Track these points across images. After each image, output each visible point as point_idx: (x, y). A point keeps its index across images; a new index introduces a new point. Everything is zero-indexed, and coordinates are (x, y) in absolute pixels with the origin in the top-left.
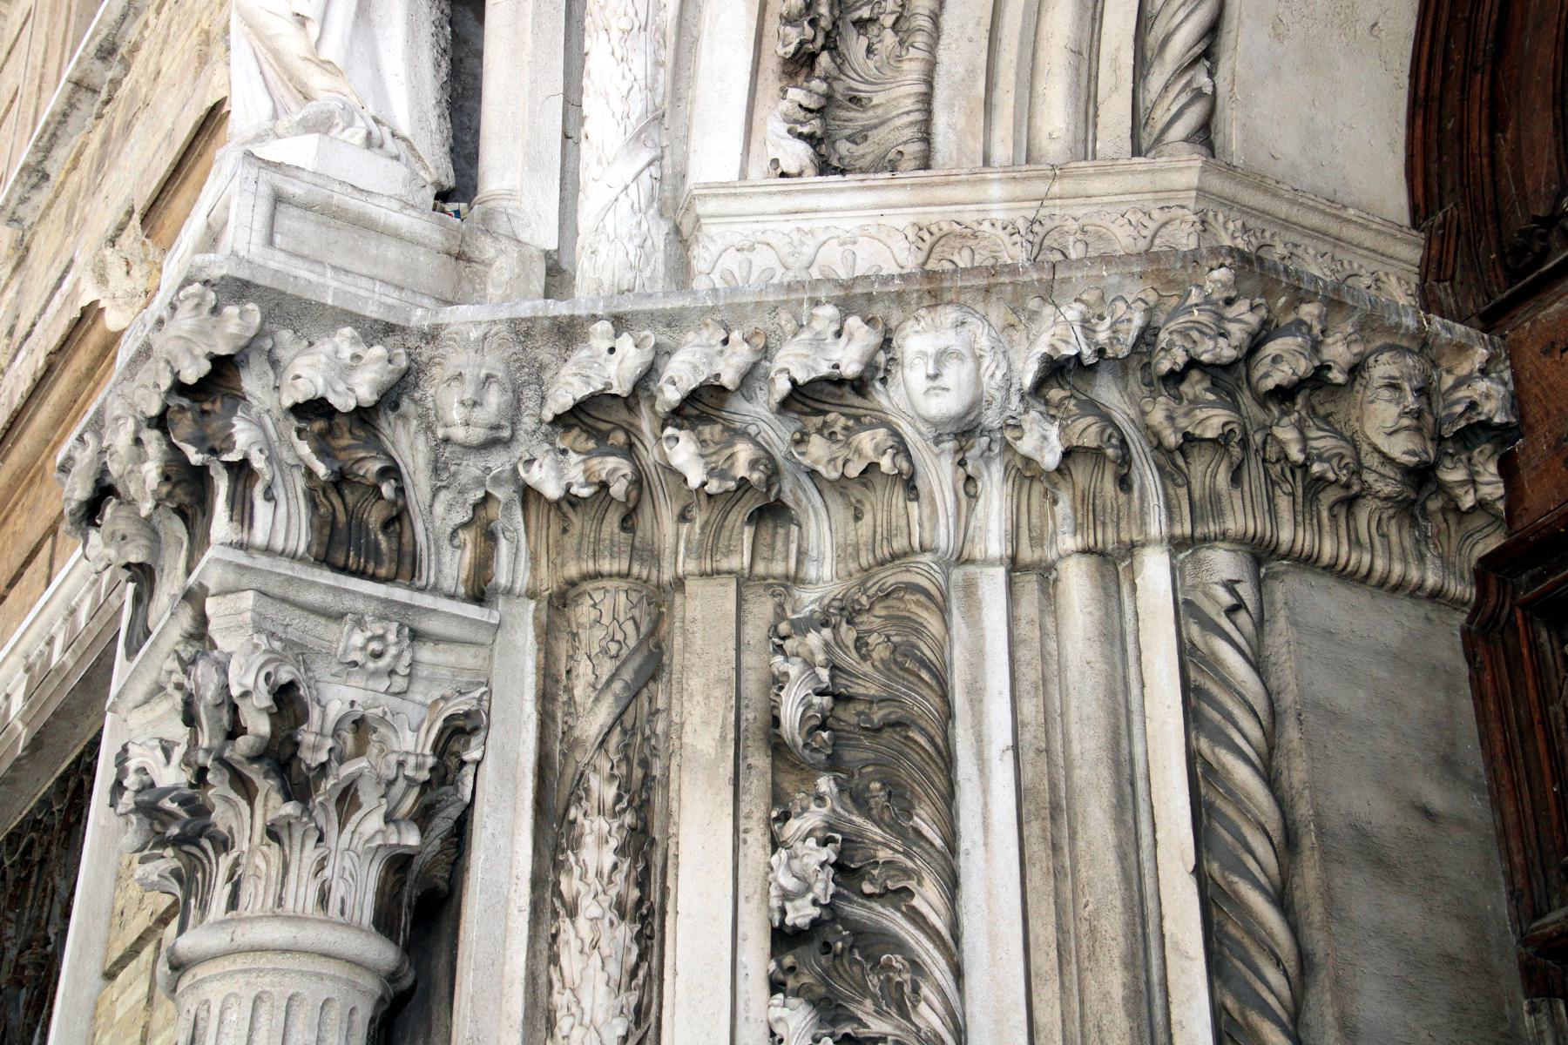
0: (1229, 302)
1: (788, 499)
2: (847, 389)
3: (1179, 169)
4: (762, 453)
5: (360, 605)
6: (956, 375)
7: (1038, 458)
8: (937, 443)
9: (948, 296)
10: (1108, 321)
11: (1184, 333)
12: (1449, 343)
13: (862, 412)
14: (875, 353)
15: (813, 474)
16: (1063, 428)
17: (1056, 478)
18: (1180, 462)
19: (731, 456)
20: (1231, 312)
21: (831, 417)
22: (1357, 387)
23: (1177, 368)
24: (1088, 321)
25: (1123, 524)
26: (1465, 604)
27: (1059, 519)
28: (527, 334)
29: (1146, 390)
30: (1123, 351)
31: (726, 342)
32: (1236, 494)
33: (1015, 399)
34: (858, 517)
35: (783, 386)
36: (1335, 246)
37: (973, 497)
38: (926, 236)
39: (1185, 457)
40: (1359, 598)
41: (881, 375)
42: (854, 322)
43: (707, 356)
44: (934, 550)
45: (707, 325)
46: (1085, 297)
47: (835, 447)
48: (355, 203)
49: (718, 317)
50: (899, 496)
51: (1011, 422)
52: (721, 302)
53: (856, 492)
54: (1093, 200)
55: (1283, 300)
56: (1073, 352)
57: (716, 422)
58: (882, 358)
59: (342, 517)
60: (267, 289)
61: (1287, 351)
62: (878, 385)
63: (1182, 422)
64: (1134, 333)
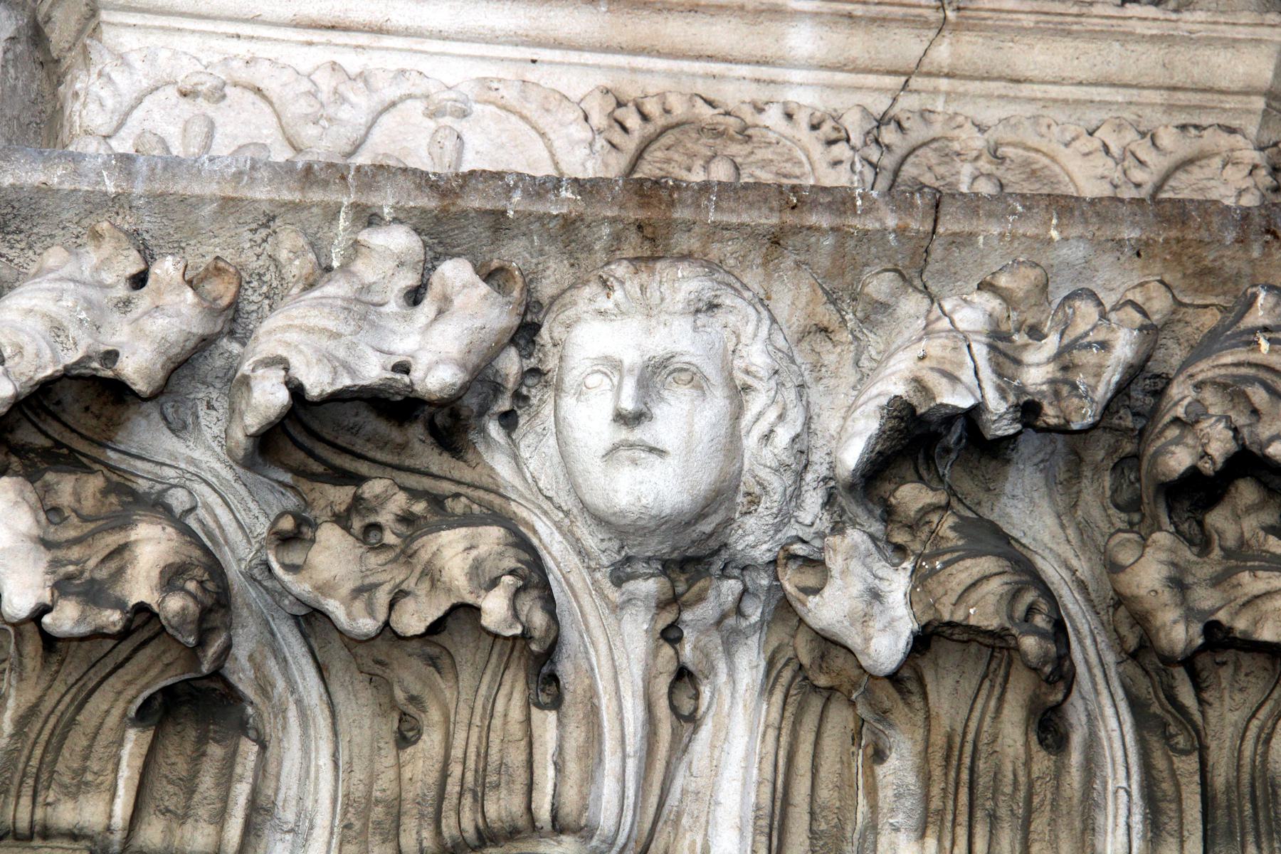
1: (243, 679)
2: (417, 431)
3: (1233, 43)
4: (197, 553)
6: (683, 421)
7: (854, 641)
8: (618, 581)
10: (1051, 343)
11: (1232, 389)
13: (448, 487)
14: (496, 351)
15: (311, 620)
16: (920, 579)
17: (887, 695)
18: (1187, 696)
19: (122, 549)
21: (374, 488)
23: (1207, 467)
24: (1007, 338)
25: (1040, 824)
27: (886, 795)
29: (1119, 519)
30: (1083, 416)
31: (139, 281)
33: (813, 500)
34: (404, 739)
35: (269, 396)
37: (689, 720)
38: (633, 121)
39: (1198, 688)
41: (504, 404)
42: (455, 273)
43: (90, 305)
44: (583, 831)
45: (97, 236)
46: (1003, 281)
47: (374, 560)
49: (127, 222)
50: (512, 698)
51: (798, 549)
52: (139, 188)
53: (409, 676)
54: (1026, 90)
56: (965, 402)
57: (90, 471)
58: (511, 364)
62: (494, 429)
63: (1205, 598)
64: (1112, 376)
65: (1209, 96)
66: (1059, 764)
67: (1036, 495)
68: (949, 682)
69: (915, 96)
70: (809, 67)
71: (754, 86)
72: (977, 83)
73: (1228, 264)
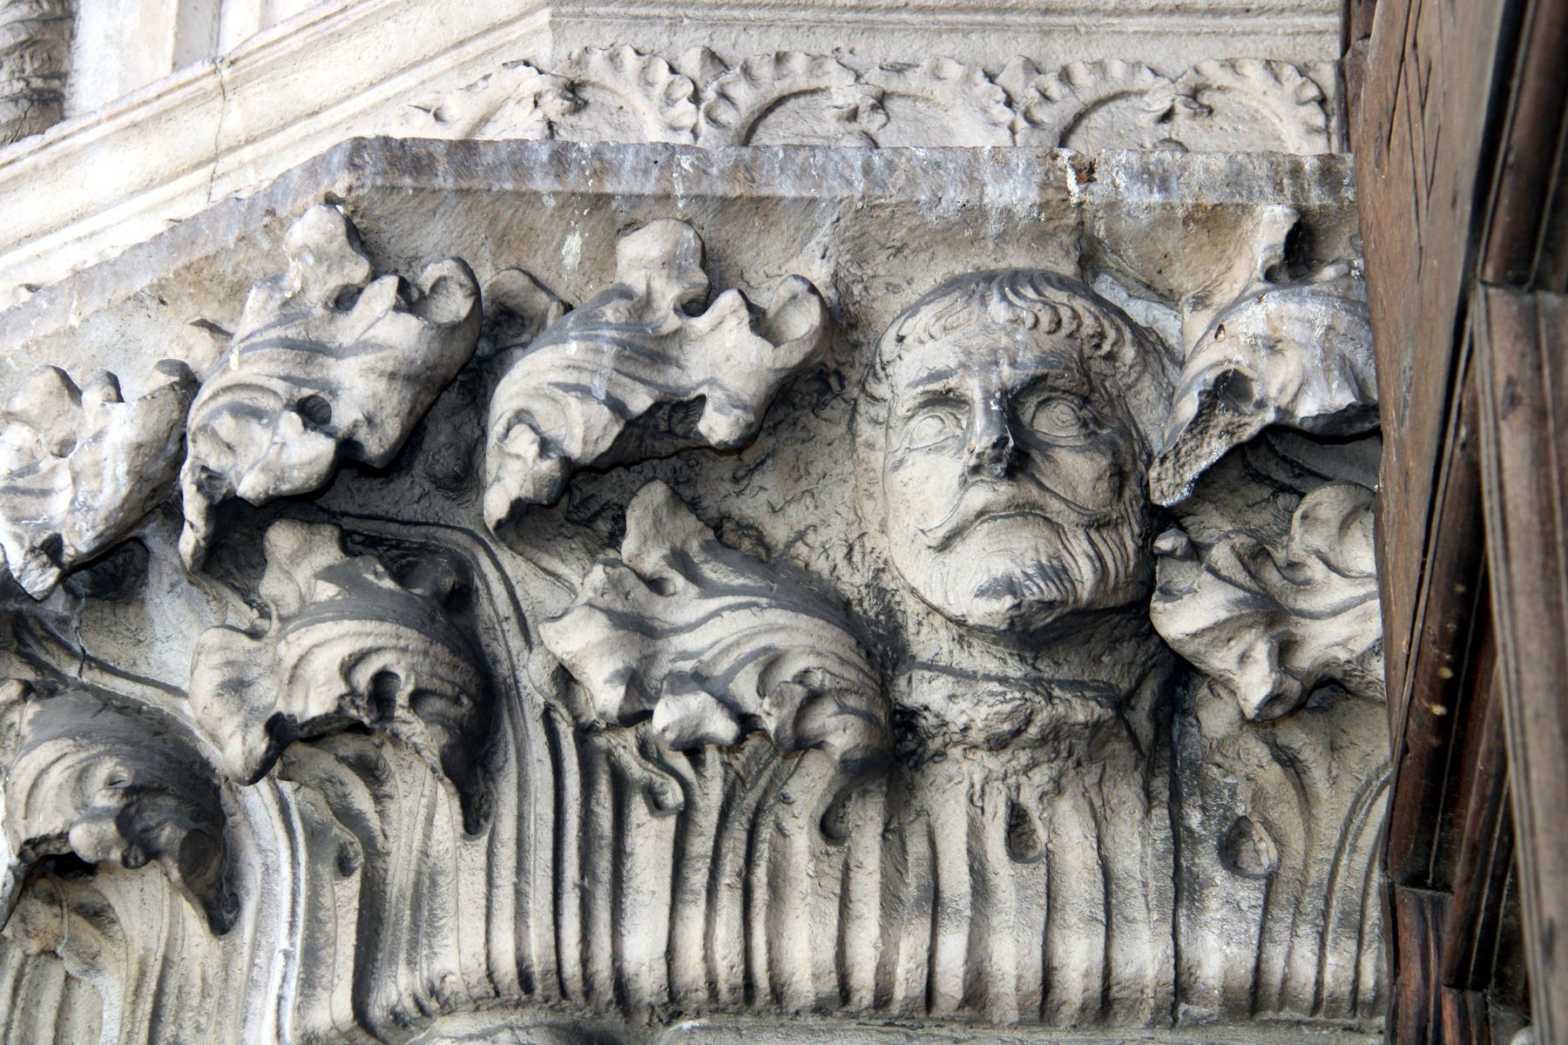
0: (345, 299)
12: (1166, 218)
18: (361, 799)
20: (349, 328)
22: (865, 431)
32: (476, 853)
36: (1046, 32)
54: (325, 119)
61: (537, 393)
65: (496, 34)
66: (229, 948)
67: (184, 627)
68: (134, 895)
69: (226, 179)
70: (122, 199)
71: (79, 245)
72: (280, 135)
73: (249, 269)
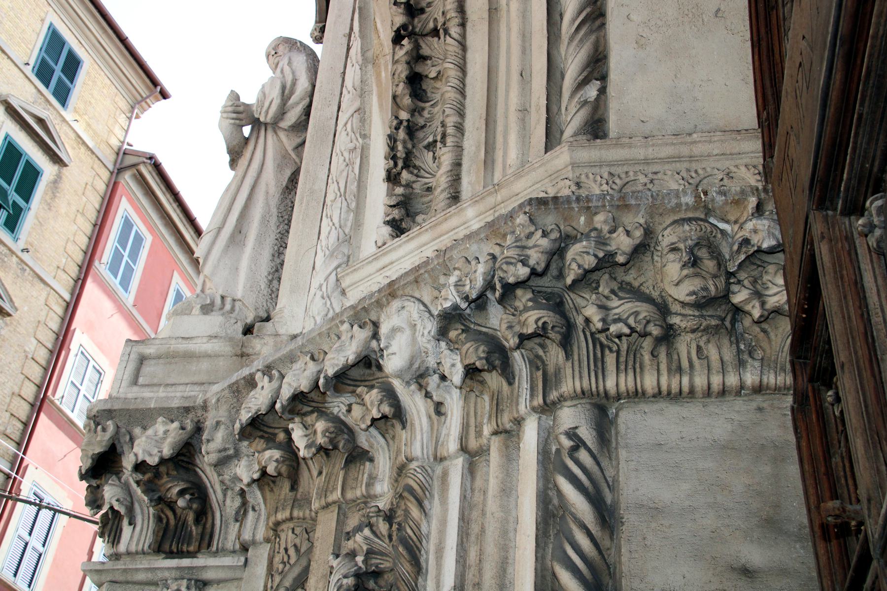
0: (529, 236)
5: (167, 574)
9: (400, 293)
12: (726, 203)
26: (788, 389)
28: (238, 391)
36: (690, 161)
40: (692, 410)
48: (183, 346)
55: (582, 219)
59: (172, 522)
60: (120, 410)
